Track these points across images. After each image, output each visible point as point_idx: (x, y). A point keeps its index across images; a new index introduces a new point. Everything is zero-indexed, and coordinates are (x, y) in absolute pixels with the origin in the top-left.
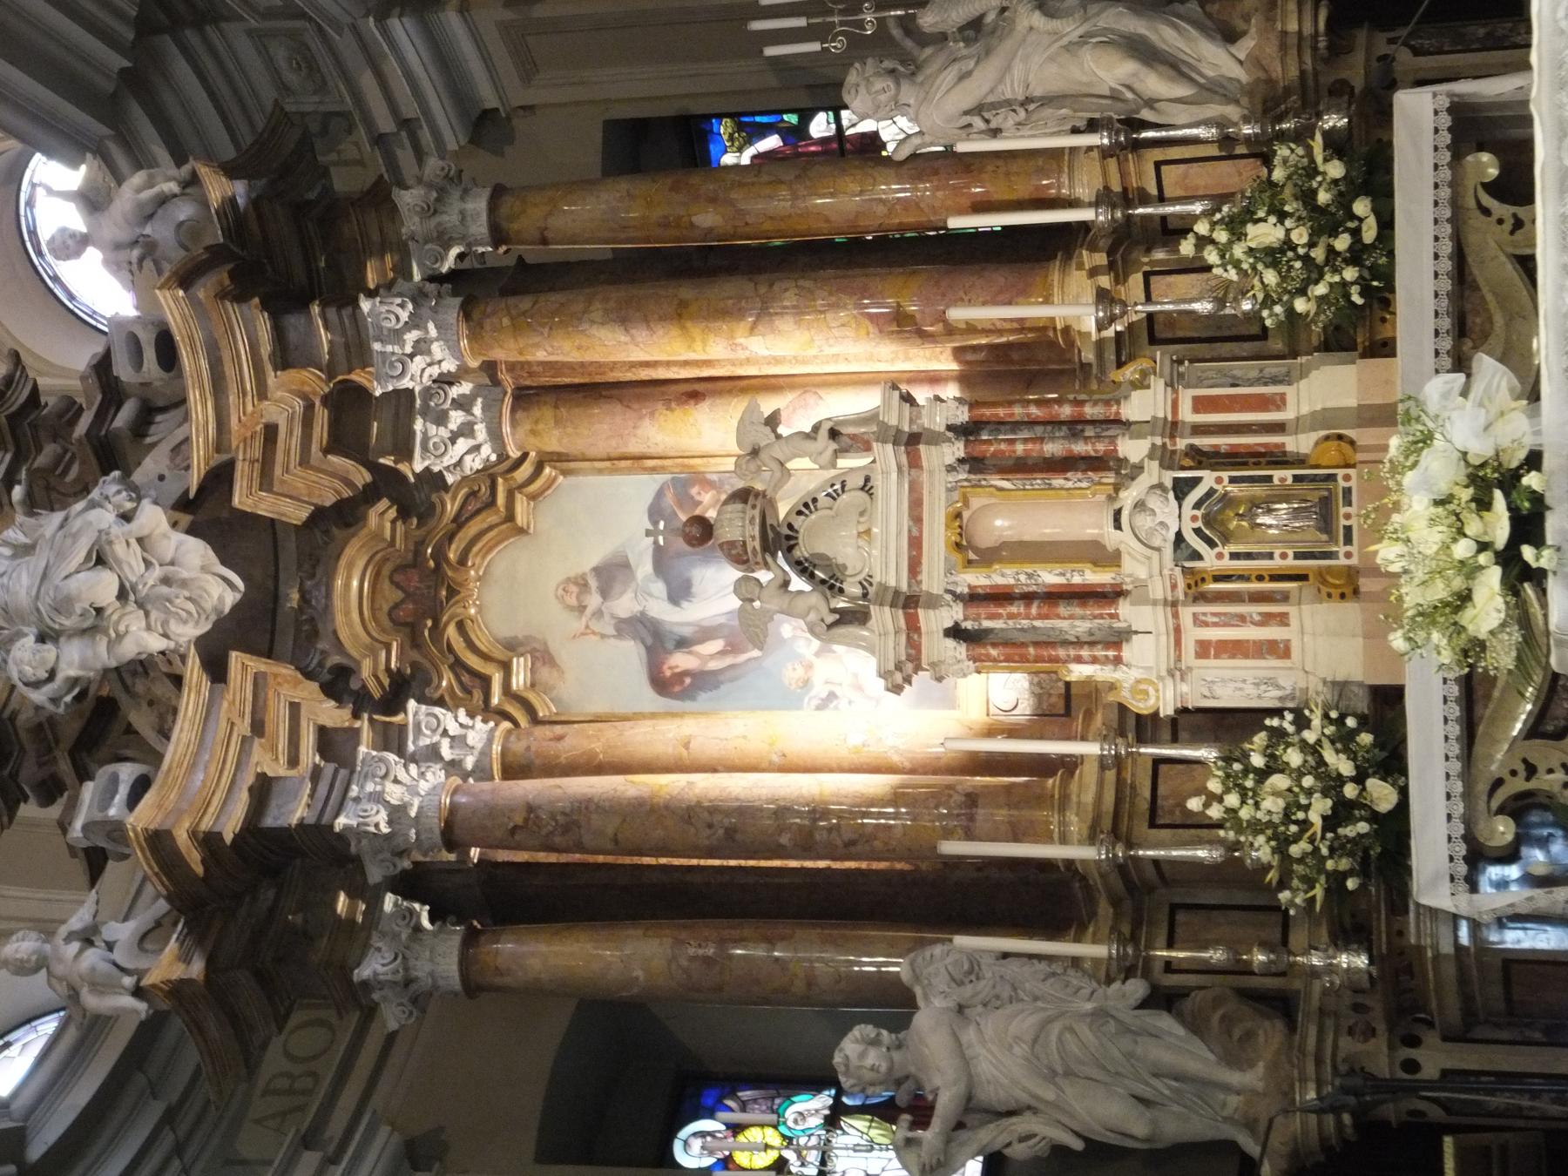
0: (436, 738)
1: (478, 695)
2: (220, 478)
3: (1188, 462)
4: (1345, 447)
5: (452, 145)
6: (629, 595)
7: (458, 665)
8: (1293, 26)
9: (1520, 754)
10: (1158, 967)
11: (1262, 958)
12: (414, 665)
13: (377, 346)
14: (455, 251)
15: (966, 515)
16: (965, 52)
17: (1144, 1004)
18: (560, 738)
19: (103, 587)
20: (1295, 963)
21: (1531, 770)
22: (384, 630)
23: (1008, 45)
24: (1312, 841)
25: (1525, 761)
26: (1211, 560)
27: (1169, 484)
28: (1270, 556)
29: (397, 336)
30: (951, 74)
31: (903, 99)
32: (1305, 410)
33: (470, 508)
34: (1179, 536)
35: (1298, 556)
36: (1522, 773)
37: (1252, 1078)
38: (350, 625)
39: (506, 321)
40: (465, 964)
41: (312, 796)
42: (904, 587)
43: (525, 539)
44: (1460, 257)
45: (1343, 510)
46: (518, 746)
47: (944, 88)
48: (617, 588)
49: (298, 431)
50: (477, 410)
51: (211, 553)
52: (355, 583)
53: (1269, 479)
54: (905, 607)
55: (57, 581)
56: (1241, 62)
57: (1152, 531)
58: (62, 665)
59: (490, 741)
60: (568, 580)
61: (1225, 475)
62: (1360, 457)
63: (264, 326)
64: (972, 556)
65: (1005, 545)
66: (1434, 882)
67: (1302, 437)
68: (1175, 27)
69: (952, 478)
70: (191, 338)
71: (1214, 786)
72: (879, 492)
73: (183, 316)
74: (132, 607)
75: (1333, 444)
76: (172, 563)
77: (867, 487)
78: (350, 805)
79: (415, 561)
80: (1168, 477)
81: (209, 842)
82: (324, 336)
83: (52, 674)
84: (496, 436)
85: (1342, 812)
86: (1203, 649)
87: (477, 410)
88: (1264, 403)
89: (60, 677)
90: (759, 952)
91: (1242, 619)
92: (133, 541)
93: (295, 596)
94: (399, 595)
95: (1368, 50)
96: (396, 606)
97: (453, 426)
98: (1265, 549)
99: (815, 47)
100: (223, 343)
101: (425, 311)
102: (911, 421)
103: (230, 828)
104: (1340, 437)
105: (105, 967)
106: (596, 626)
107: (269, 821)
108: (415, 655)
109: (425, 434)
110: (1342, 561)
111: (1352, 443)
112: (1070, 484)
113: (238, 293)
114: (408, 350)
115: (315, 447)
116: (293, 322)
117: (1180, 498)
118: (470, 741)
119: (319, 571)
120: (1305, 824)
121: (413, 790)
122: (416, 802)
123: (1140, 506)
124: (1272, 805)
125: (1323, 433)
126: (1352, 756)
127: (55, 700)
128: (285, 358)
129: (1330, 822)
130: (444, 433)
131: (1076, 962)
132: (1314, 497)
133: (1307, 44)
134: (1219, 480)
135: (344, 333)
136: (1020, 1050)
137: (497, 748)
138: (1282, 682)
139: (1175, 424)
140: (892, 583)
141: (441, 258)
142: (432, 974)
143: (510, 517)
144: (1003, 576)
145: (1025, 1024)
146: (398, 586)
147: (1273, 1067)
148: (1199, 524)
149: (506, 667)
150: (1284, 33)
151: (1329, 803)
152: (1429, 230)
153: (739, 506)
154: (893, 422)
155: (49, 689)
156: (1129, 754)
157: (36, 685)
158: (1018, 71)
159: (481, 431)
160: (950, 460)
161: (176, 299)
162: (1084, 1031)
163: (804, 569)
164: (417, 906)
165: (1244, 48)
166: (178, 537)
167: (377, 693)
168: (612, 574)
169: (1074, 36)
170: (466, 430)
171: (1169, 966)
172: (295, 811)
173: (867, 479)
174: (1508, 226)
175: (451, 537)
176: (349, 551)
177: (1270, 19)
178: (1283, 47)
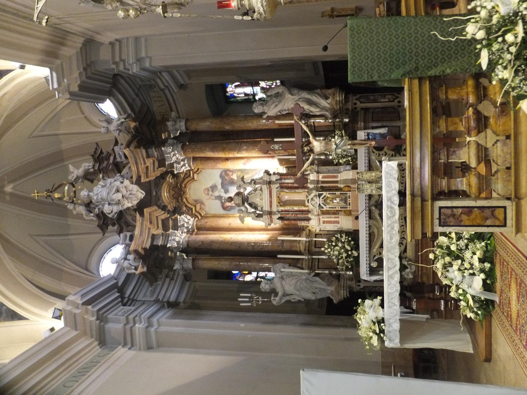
0: (184, 223)
1: (190, 211)
2: (139, 177)
3: (321, 190)
4: (349, 188)
5: (176, 91)
6: (217, 192)
7: (186, 206)
8: (338, 99)
11: (334, 272)
12: (178, 206)
13: (166, 155)
14: (179, 132)
15: (280, 196)
16: (276, 100)
18: (206, 223)
19: (119, 196)
20: (340, 274)
22: (172, 199)
23: (284, 100)
24: (343, 260)
25: (385, 152)
26: (325, 208)
27: (317, 194)
28: (336, 208)
29: (170, 153)
30: (273, 106)
33: (186, 176)
34: (319, 204)
35: (341, 208)
36: (379, 254)
38: (165, 199)
39: (190, 150)
40: (193, 265)
41: (162, 239)
42: (269, 210)
43: (196, 181)
44: (369, 161)
46: (199, 224)
47: (272, 108)
48: (215, 191)
49: (152, 166)
50: (186, 162)
51: (138, 188)
52: (166, 194)
53: (335, 194)
54: (270, 214)
55: (111, 196)
56: (328, 104)
58: (114, 210)
59: (194, 223)
60: (205, 189)
61: (328, 193)
62: (351, 190)
63: (144, 151)
64: (281, 204)
66: (364, 274)
68: (316, 96)
69: (277, 189)
70: (131, 156)
71: (326, 247)
72: (263, 190)
73: (129, 153)
74: (125, 199)
76: (131, 191)
77: (261, 190)
78: (169, 242)
79: (176, 186)
80: (317, 193)
81: (145, 249)
82: (156, 153)
83: (112, 212)
84: (190, 166)
85: (348, 256)
87: (186, 162)
89: (113, 212)
90: (246, 264)
91: (331, 217)
92: (124, 188)
93: (154, 193)
94: (174, 192)
95: (352, 101)
96: (174, 194)
97: (182, 165)
98: (335, 207)
99: (250, 304)
100: (137, 156)
101: (175, 148)
102: (269, 179)
103: (148, 246)
104: (348, 186)
106: (211, 197)
107: (155, 243)
108: (178, 204)
109: (176, 166)
110: (348, 209)
111: (350, 187)
112: (299, 191)
113: (138, 147)
114: (172, 156)
115: (156, 168)
116: (150, 151)
117: (319, 198)
118: (190, 223)
119: (159, 188)
120: (342, 257)
121: (180, 238)
122: (181, 241)
123: (312, 199)
124: (336, 253)
125: (345, 185)
126: (350, 246)
127: (113, 216)
128: (148, 156)
129: (346, 258)
130: (180, 166)
132: (344, 197)
133: (341, 102)
134: (326, 194)
135: (159, 152)
136: (293, 286)
137: (195, 223)
139: (318, 181)
140: (267, 210)
141: (177, 133)
142: (187, 267)
143: (193, 178)
144: (287, 208)
145: (294, 282)
146: (173, 191)
148: (323, 202)
149: (195, 206)
150: (336, 101)
151: (346, 254)
152: (364, 158)
153: (237, 197)
154: (266, 179)
155: (112, 214)
156: (311, 240)
157: (109, 214)
158: (286, 105)
159: (187, 165)
160: (276, 187)
161: (127, 150)
162: (304, 283)
163: (251, 205)
164: (183, 254)
165: (329, 101)
166: (132, 185)
167: (171, 210)
168: (214, 188)
169: (297, 99)
170: (184, 165)
172: (160, 242)
173: (261, 188)
174: (378, 155)
175: (183, 182)
176: (164, 185)
177: (334, 98)
178: (336, 104)
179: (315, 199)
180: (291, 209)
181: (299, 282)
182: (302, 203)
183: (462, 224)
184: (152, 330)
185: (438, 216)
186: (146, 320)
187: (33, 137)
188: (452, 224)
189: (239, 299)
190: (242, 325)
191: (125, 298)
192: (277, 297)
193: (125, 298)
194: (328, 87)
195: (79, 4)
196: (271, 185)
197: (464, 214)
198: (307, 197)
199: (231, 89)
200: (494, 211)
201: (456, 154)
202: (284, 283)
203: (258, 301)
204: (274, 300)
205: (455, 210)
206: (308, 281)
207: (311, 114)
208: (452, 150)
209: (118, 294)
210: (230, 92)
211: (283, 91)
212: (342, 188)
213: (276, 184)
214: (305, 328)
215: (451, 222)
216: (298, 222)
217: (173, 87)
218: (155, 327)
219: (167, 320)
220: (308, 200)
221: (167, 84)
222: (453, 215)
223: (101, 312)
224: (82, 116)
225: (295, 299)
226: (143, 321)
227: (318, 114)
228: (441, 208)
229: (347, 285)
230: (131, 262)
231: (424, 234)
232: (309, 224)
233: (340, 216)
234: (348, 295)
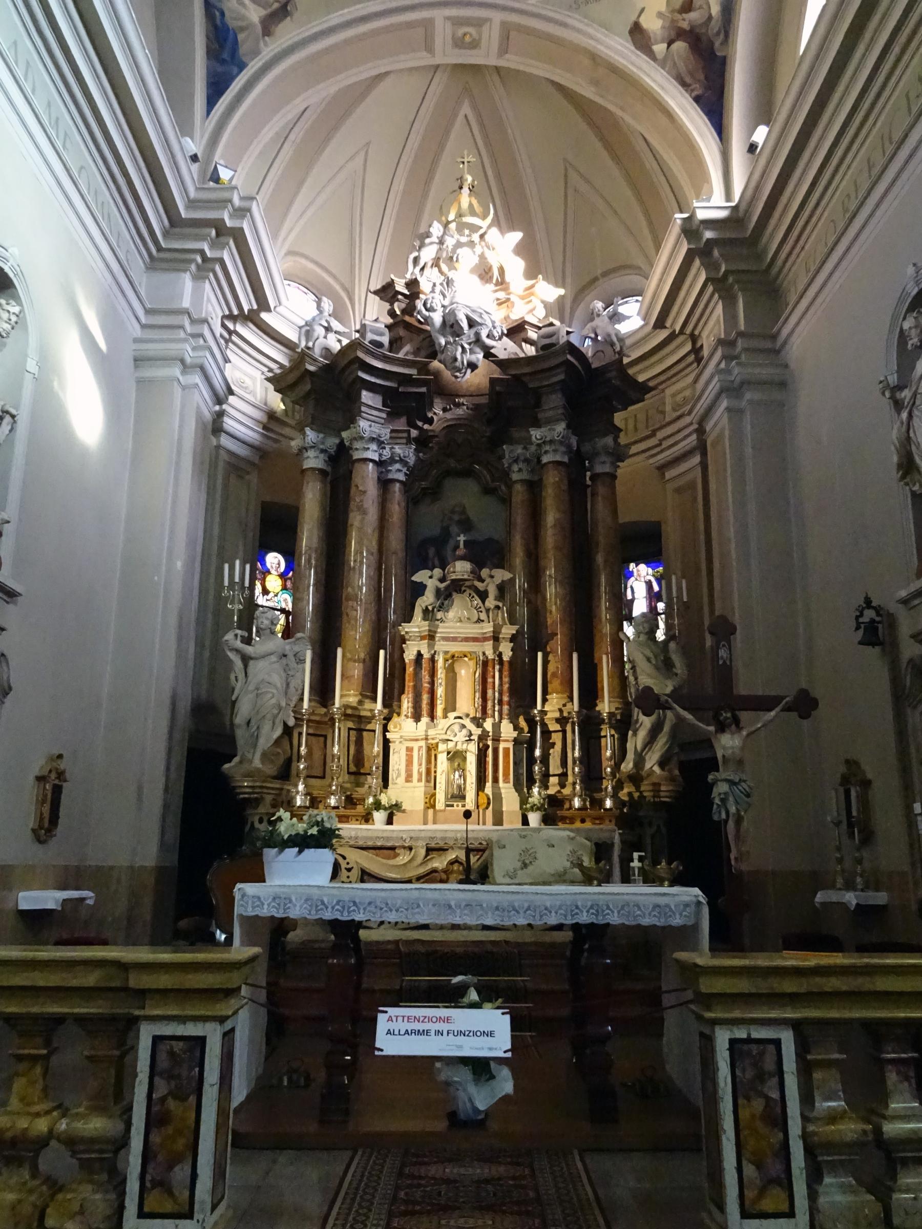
4: (485, 805)
9: (355, 866)
10: (299, 730)
11: (302, 767)
15: (466, 659)
17: (285, 724)
21: (349, 870)
30: (651, 655)
31: (642, 635)
32: (503, 791)
37: (257, 763)
45: (460, 804)
47: (645, 652)
57: (453, 731)
60: (464, 508)
65: (455, 674)
67: (490, 789)
68: (667, 742)
69: (481, 654)
72: (477, 625)
75: (486, 801)
86: (409, 750)
88: (506, 775)
91: (420, 765)
99: (226, 583)
104: (489, 804)
105: (316, 335)
111: (487, 808)
123: (463, 726)
125: (491, 797)
127: (419, 312)
131: (302, 699)
138: (399, 779)
140: (439, 630)
144: (441, 674)
147: (258, 770)
160: (487, 653)
162: (273, 701)
165: (656, 769)
171: (300, 734)
179: (464, 732)
180: (440, 681)
181: (275, 691)
182: (451, 706)
183: (741, 1101)
184: (176, 371)
185: (755, 1035)
186: (198, 361)
187: (566, 169)
188: (738, 1073)
189: (238, 563)
190: (179, 564)
191: (235, 324)
192: (242, 642)
193: (235, 324)
194: (682, 766)
195: (914, 265)
196: (491, 642)
197: (767, 1106)
198: (467, 715)
199: (643, 573)
200: (780, 1185)
201: (901, 1082)
202: (273, 658)
203: (232, 603)
204: (236, 635)
205: (775, 1081)
206: (276, 712)
207: (630, 733)
208: (912, 1074)
209: (246, 308)
210: (638, 571)
211: (676, 674)
212: (483, 791)
213: (495, 652)
214: (167, 702)
215: (744, 1071)
216: (410, 696)
217: (659, 457)
218: (181, 378)
219: (195, 405)
220: (460, 718)
221: (665, 444)
222: (761, 1077)
223: (218, 268)
224: (599, 272)
225: (237, 680)
226: (196, 354)
227: (630, 746)
228: (777, 1043)
229: (264, 796)
230: (321, 340)
231: (708, 1000)
232: (403, 717)
233: (423, 784)
234: (242, 796)
